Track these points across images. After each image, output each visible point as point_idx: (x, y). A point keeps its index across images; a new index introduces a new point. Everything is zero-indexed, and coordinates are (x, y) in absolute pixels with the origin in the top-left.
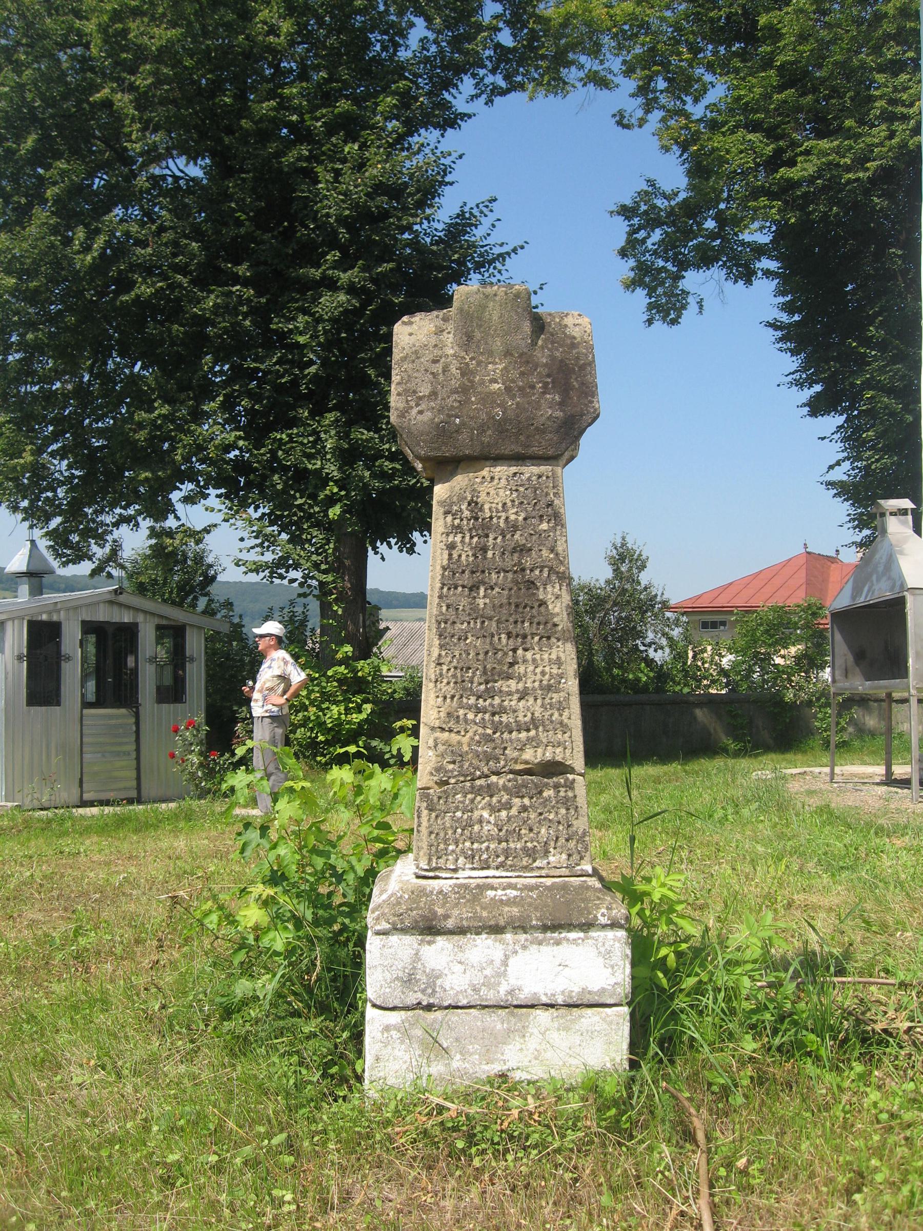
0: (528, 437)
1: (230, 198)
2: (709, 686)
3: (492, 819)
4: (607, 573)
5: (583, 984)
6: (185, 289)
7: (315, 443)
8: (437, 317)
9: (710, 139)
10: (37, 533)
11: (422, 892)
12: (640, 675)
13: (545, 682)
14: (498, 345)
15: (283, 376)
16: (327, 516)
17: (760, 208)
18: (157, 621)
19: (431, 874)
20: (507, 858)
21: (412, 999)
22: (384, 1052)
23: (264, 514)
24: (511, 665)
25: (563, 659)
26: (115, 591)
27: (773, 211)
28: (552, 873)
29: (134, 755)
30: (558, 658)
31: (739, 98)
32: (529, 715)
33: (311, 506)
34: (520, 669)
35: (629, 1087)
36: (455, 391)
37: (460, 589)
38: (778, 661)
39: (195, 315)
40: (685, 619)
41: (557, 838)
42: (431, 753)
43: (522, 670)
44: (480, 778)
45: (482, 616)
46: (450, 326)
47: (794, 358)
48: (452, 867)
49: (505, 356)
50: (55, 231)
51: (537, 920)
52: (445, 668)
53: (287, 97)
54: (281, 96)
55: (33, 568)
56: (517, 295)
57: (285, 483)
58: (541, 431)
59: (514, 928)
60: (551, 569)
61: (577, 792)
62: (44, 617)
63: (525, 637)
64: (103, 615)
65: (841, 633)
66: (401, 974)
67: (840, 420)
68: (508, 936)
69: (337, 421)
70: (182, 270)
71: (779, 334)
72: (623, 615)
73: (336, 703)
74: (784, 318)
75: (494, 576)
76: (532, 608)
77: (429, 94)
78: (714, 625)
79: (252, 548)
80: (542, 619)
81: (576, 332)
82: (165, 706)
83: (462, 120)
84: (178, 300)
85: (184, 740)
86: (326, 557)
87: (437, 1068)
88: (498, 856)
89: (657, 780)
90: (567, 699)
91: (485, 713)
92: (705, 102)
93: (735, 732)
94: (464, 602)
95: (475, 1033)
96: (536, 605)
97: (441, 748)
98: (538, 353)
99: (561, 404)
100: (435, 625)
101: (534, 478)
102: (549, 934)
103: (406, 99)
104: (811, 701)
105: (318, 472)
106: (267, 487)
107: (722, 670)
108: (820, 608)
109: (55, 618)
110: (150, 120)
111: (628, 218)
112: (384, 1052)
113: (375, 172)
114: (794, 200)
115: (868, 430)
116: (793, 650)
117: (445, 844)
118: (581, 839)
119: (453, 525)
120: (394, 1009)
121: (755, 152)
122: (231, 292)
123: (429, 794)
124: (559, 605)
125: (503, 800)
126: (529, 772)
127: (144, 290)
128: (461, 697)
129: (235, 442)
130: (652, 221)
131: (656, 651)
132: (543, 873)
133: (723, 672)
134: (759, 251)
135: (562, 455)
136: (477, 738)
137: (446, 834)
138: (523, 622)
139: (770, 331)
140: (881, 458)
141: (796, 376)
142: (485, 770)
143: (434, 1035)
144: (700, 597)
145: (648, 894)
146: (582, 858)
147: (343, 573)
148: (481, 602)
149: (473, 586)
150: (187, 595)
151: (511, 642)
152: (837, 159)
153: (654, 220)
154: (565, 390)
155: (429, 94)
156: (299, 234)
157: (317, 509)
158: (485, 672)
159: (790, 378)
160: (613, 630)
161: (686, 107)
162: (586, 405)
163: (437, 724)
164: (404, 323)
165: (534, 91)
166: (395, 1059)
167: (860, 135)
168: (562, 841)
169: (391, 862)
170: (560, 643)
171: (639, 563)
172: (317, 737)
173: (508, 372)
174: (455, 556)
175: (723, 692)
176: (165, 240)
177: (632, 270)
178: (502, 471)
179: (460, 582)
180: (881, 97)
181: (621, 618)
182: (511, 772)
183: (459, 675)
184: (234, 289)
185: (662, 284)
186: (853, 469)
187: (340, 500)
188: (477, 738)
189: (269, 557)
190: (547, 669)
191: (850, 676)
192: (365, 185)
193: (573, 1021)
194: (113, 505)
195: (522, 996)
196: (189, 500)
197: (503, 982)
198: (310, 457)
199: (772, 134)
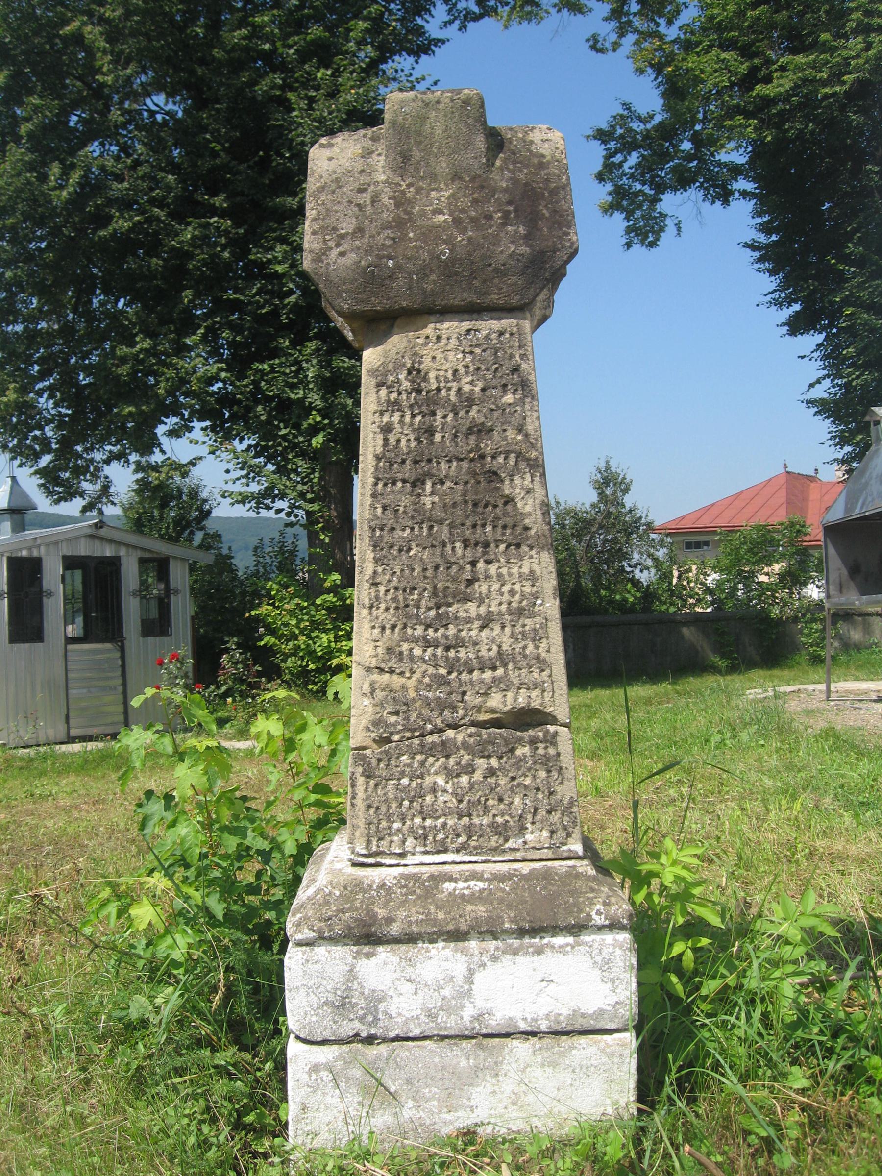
0: (485, 281)
1: (204, 129)
2: (695, 605)
3: (449, 787)
4: (594, 497)
5: (573, 1005)
6: (163, 222)
7: (297, 373)
8: (365, 136)
9: (684, 60)
10: (27, 471)
11: (358, 886)
12: (627, 596)
13: (515, 605)
14: (443, 166)
15: (263, 307)
16: (310, 445)
17: (736, 127)
18: (140, 554)
19: (371, 860)
20: (470, 837)
21: (347, 1029)
22: (312, 1100)
23: (250, 446)
24: (470, 582)
25: (538, 573)
26: (96, 524)
27: (749, 130)
28: (531, 855)
29: (120, 689)
30: (532, 572)
31: (712, 18)
32: (495, 648)
33: (295, 437)
34: (482, 587)
35: (637, 1141)
36: (384, 227)
37: (399, 484)
38: (763, 578)
39: (174, 247)
40: (669, 539)
41: (536, 810)
42: (366, 702)
43: (484, 589)
44: (431, 733)
45: (430, 520)
46: (381, 147)
47: (773, 278)
48: (398, 851)
49: (453, 180)
50: (31, 167)
51: (511, 922)
52: (382, 589)
53: (259, 26)
54: (253, 25)
55: (14, 505)
56: (467, 102)
57: (269, 414)
58: (501, 273)
59: (480, 933)
60: (519, 455)
61: (561, 748)
62: (25, 553)
63: (486, 545)
64: (83, 549)
65: (835, 546)
66: (331, 997)
67: (820, 338)
68: (473, 944)
69: (318, 350)
70: (160, 203)
71: (757, 254)
72: (609, 537)
73: (326, 631)
74: (762, 238)
75: (444, 466)
76: (495, 506)
77: (402, 20)
78: (698, 545)
79: (238, 479)
80: (509, 521)
81: (545, 150)
82: (150, 640)
83: (436, 45)
84: (156, 233)
85: (169, 673)
86: (312, 486)
87: (382, 1120)
88: (458, 836)
89: (648, 702)
90: (545, 626)
91: (436, 647)
92: (678, 23)
93: (721, 650)
94: (405, 501)
95: (432, 1072)
96: (500, 502)
97: (380, 695)
98: (495, 176)
99: (527, 237)
100: (368, 533)
101: (494, 336)
102: (527, 940)
103: (378, 24)
104: (796, 617)
105: (301, 401)
106: (251, 418)
107: (708, 588)
108: (803, 526)
109: (35, 554)
110: (122, 52)
111: (604, 142)
112: (312, 1100)
113: (348, 97)
114: (770, 119)
115: (848, 347)
116: (777, 567)
117: (388, 820)
118: (568, 810)
119: (388, 401)
120: (324, 1042)
121: (730, 71)
122: (209, 224)
123: (365, 756)
124: (530, 501)
125: (464, 762)
126: (496, 724)
127: (121, 224)
128: (405, 626)
129: (217, 374)
130: (628, 144)
131: (641, 571)
132: (519, 855)
133: (709, 591)
134: (736, 171)
135: (533, 301)
136: (427, 680)
137: (389, 807)
138: (484, 526)
139: (748, 251)
140: (862, 374)
141: (776, 295)
142: (439, 722)
143: (378, 1075)
144: (683, 518)
145: (656, 875)
146: (569, 835)
147: (330, 502)
148: (427, 501)
149: (418, 480)
150: (184, 529)
151: (469, 552)
152: (814, 74)
153: (630, 143)
154: (533, 220)
155: (402, 20)
156: (274, 164)
157: (301, 439)
158: (435, 593)
159: (768, 298)
160: (599, 552)
161: (660, 29)
162: (560, 238)
163: (374, 664)
164: (323, 146)
165: (509, 18)
166: (327, 1108)
167: (836, 48)
168: (542, 813)
169: (330, 834)
170: (533, 552)
171: (623, 486)
172: (307, 665)
173: (457, 200)
174: (392, 441)
175: (709, 610)
176: (140, 174)
177: (610, 194)
178: (451, 327)
179: (400, 476)
180: (857, 9)
181: (607, 540)
182: (473, 724)
183: (401, 598)
184: (212, 221)
185: (640, 207)
186: (834, 387)
187: (323, 429)
188: (427, 680)
189: (254, 488)
190: (517, 587)
191: (844, 591)
192: (339, 111)
193: (561, 1054)
194: (103, 440)
195: (493, 1023)
196: (174, 433)
197: (468, 1004)
198: (293, 386)
199: (746, 52)
